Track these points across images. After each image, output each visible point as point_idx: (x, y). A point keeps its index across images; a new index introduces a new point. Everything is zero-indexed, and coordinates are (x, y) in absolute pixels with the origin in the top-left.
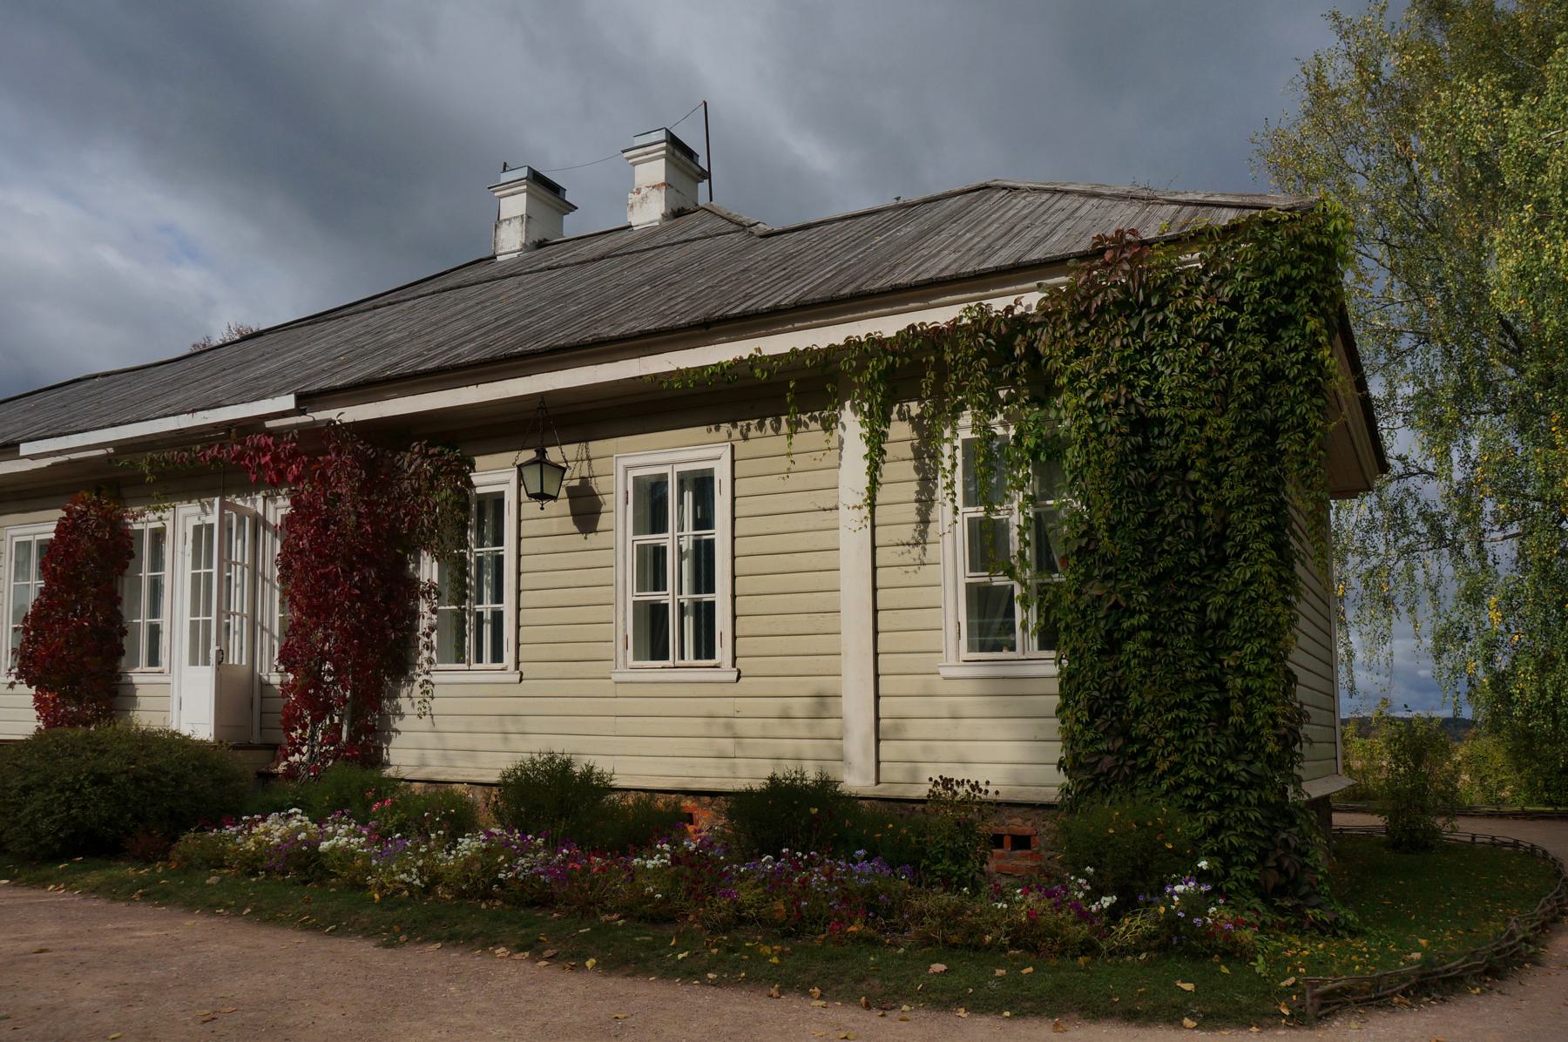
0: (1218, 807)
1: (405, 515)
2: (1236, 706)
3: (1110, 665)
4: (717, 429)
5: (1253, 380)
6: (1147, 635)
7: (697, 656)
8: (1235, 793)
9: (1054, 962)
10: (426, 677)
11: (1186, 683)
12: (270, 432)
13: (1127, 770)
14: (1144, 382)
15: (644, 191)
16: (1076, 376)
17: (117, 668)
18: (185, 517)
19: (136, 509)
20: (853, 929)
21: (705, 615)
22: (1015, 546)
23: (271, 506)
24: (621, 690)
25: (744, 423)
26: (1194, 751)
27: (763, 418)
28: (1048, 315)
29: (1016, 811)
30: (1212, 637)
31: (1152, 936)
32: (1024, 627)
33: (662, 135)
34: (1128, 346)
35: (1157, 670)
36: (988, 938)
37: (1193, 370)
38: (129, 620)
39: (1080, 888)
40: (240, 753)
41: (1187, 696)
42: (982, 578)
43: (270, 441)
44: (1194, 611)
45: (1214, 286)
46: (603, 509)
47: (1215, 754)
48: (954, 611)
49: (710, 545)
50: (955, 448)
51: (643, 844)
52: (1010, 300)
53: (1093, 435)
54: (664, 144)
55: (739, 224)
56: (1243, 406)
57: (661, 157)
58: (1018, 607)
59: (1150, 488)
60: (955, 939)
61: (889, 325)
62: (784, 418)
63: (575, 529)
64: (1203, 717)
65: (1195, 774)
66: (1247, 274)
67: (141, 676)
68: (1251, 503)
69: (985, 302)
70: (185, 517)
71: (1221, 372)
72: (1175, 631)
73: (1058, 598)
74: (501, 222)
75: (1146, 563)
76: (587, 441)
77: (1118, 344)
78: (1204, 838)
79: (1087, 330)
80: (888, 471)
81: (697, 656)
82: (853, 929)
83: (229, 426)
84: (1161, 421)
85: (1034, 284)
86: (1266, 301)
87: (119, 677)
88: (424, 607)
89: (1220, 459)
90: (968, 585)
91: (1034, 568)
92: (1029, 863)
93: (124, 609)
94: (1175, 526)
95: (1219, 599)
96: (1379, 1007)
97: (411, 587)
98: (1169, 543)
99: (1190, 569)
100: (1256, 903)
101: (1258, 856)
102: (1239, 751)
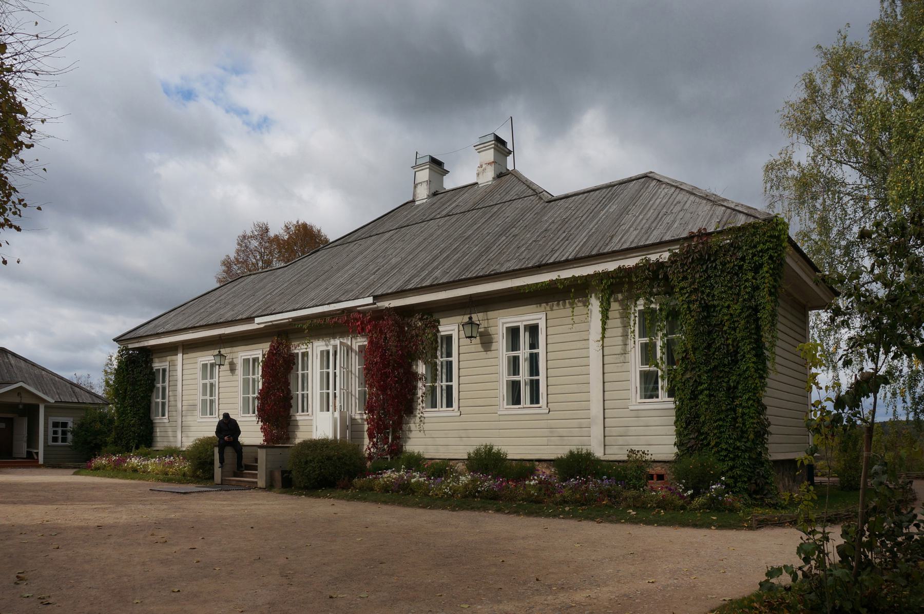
0: (733, 459)
1: (413, 345)
2: (740, 420)
3: (693, 404)
4: (540, 306)
5: (749, 290)
6: (706, 392)
7: (532, 403)
8: (740, 454)
9: (671, 512)
10: (421, 415)
11: (722, 411)
12: (359, 312)
13: (699, 445)
14: (708, 291)
15: (484, 166)
16: (682, 289)
17: (289, 414)
18: (317, 347)
19: (296, 343)
20: (604, 502)
21: (534, 386)
22: (659, 354)
23: (354, 341)
24: (502, 418)
25: (551, 303)
26: (724, 438)
27: (559, 301)
28: (673, 261)
29: (658, 464)
30: (733, 392)
31: (705, 504)
32: (662, 388)
33: (492, 138)
34: (702, 276)
35: (712, 406)
36: (649, 505)
37: (726, 286)
38: (293, 393)
39: (681, 488)
40: (226, 461)
41: (722, 416)
42: (646, 368)
43: (361, 316)
44: (726, 382)
45: (735, 252)
46: (494, 341)
47: (732, 439)
48: (635, 381)
49: (537, 355)
50: (636, 317)
51: (526, 477)
52: (657, 256)
53: (688, 312)
54: (493, 142)
55: (534, 190)
56: (744, 300)
58: (660, 380)
59: (710, 333)
60: (638, 505)
61: (611, 266)
62: (567, 301)
63: (483, 350)
64: (728, 424)
65: (724, 446)
66: (747, 247)
67: (300, 417)
68: (747, 339)
69: (648, 256)
70: (317, 347)
71: (737, 286)
72: (719, 390)
73: (675, 377)
74: (417, 184)
75: (707, 363)
76: (487, 312)
77: (698, 276)
78: (727, 471)
79: (687, 270)
80: (610, 323)
81: (532, 403)
82: (604, 502)
83: (343, 310)
84: (714, 306)
85: (666, 249)
86: (754, 258)
87: (290, 417)
88: (420, 384)
89: (736, 321)
90: (641, 371)
91: (666, 364)
93: (292, 387)
94: (719, 348)
95: (734, 378)
96: (779, 526)
97: (415, 377)
98: (717, 355)
99: (725, 365)
100: (746, 496)
101: (748, 478)
102: (742, 437)
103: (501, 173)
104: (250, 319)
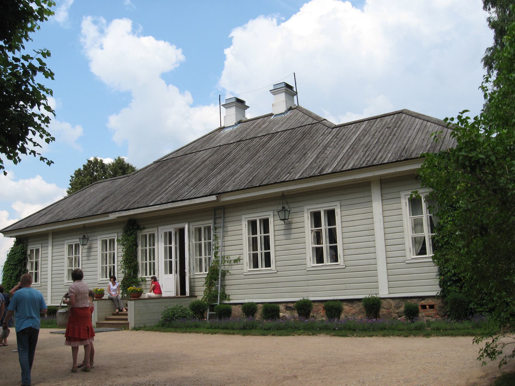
21: (268, 256)
42: (69, 268)
57: (282, 92)
92: (434, 312)
103: (241, 120)
104: (106, 213)
